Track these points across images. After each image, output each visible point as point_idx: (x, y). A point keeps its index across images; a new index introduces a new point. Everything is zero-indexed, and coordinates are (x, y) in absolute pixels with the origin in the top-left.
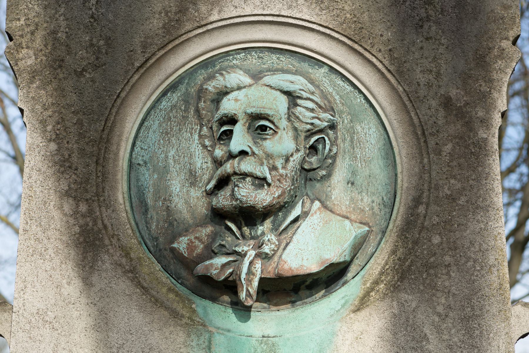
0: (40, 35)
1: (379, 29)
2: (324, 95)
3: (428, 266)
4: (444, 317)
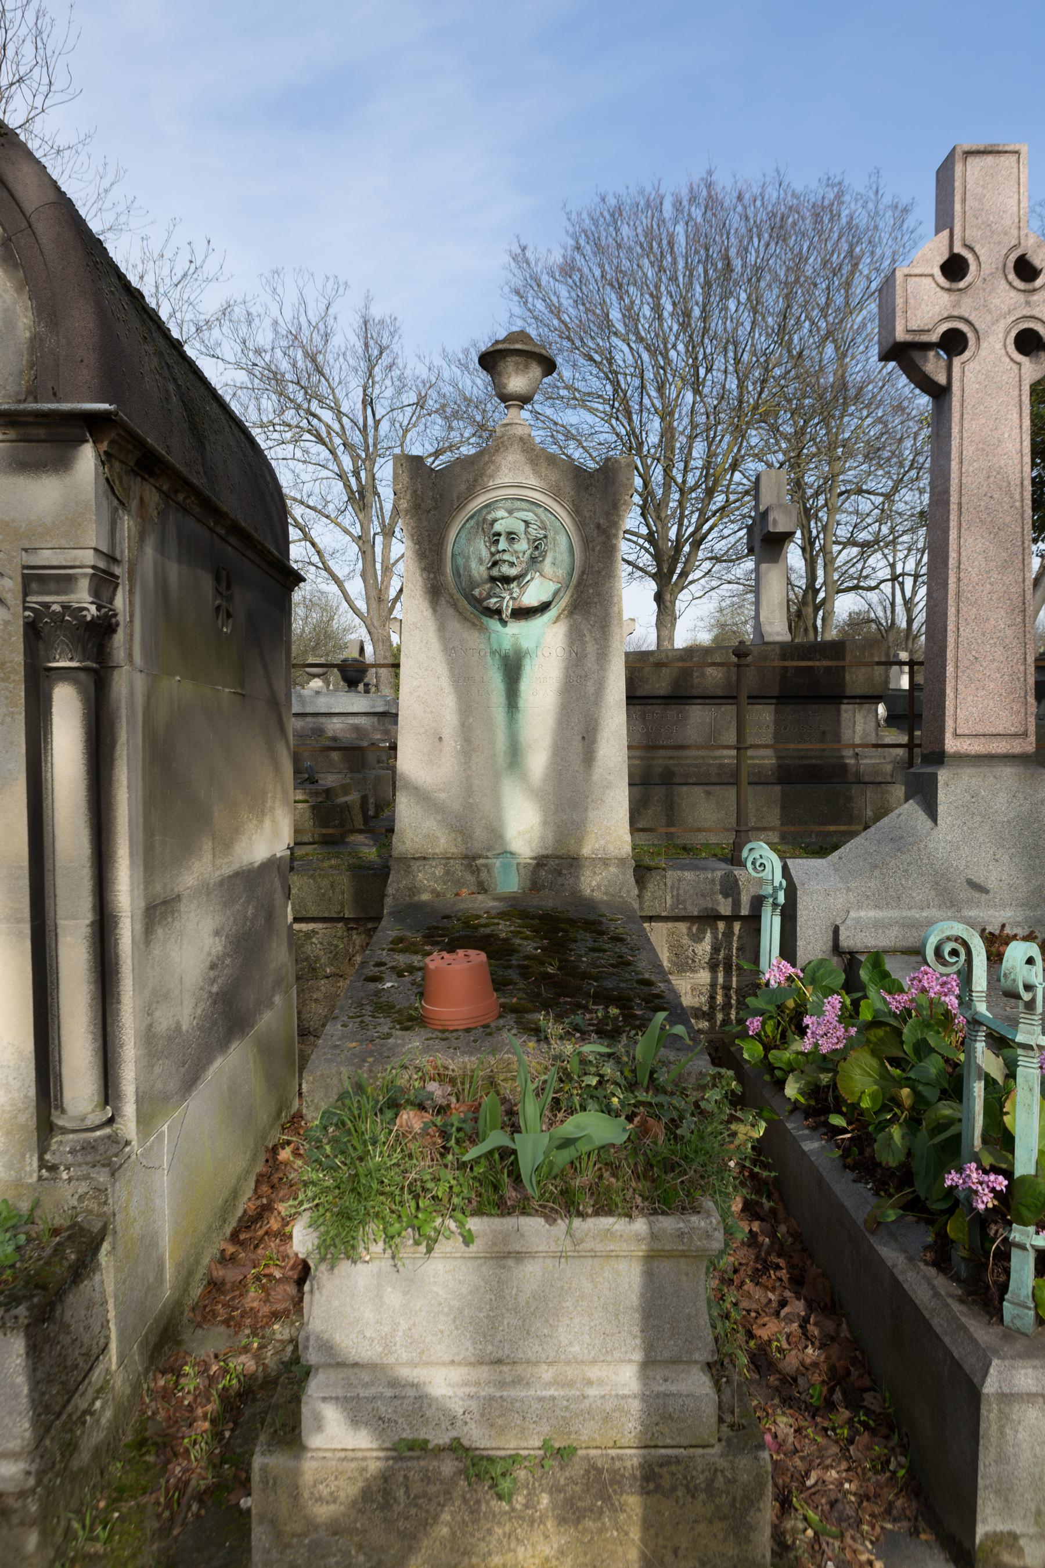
0: (409, 492)
1: (568, 490)
2: (542, 522)
3: (587, 603)
4: (593, 626)
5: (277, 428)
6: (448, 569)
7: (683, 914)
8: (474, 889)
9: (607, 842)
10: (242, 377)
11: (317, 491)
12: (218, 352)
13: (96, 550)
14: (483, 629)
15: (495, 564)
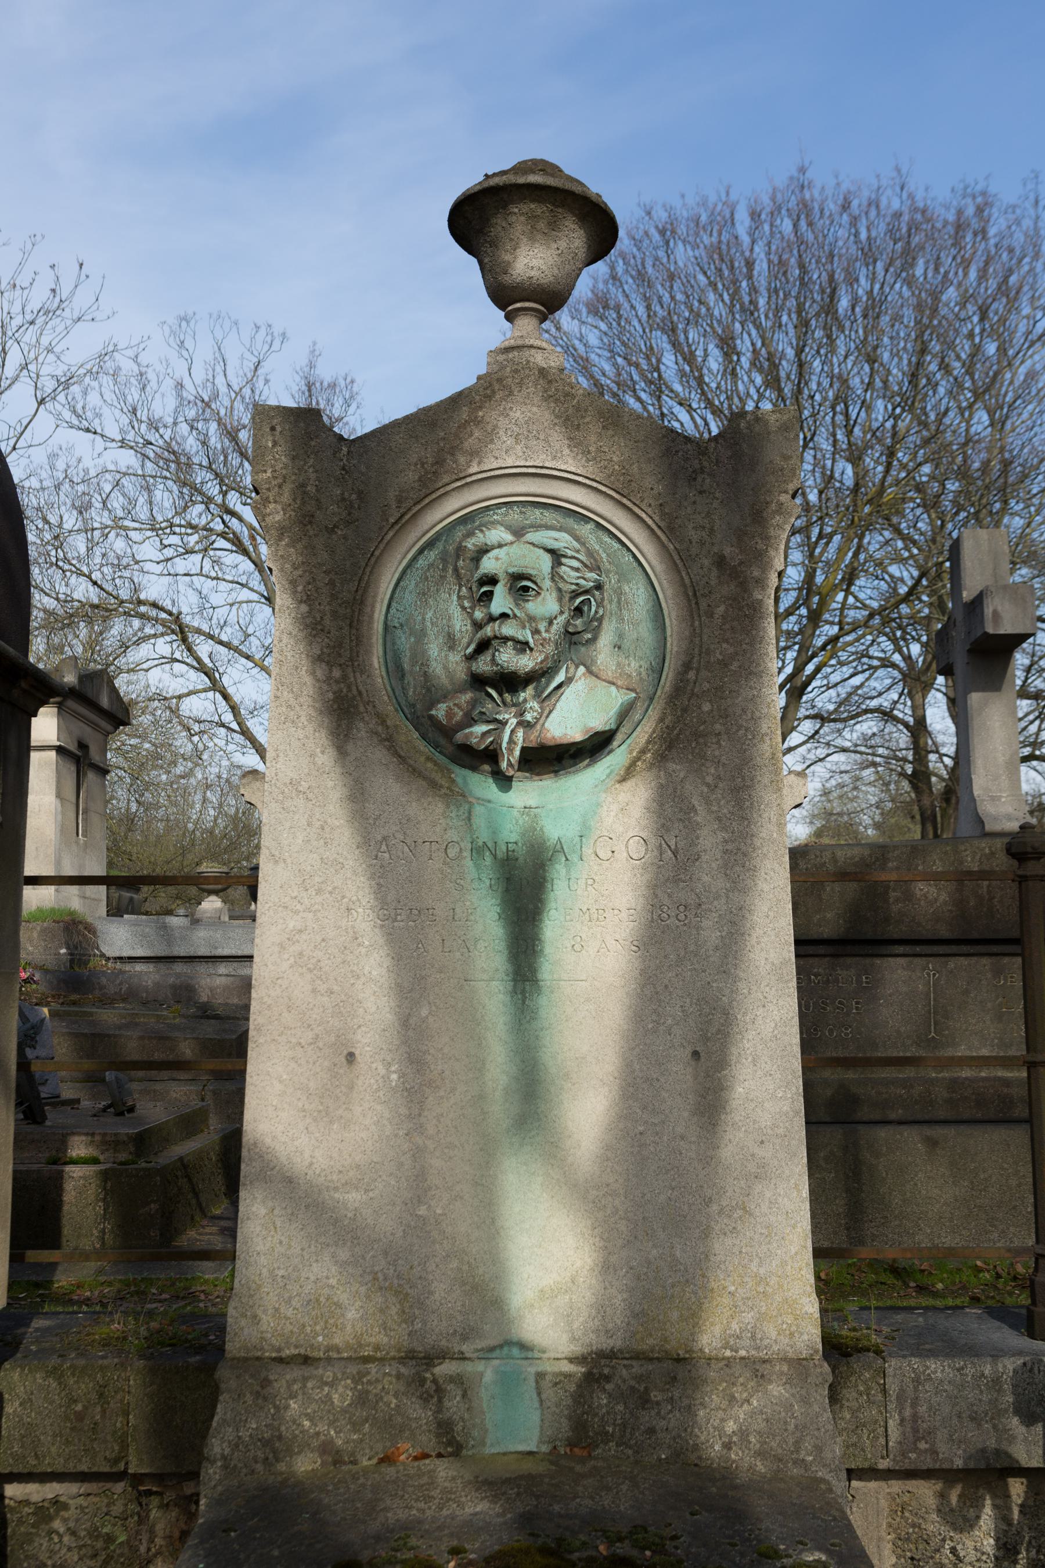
1: (649, 482)
2: (590, 553)
3: (697, 735)
5: (177, 530)
6: (376, 660)
7: (928, 1463)
8: (428, 1441)
9: (761, 1317)
10: (127, 459)
11: (233, 618)
12: (96, 425)
13: (60, 750)
14: (455, 796)
15: (483, 646)
